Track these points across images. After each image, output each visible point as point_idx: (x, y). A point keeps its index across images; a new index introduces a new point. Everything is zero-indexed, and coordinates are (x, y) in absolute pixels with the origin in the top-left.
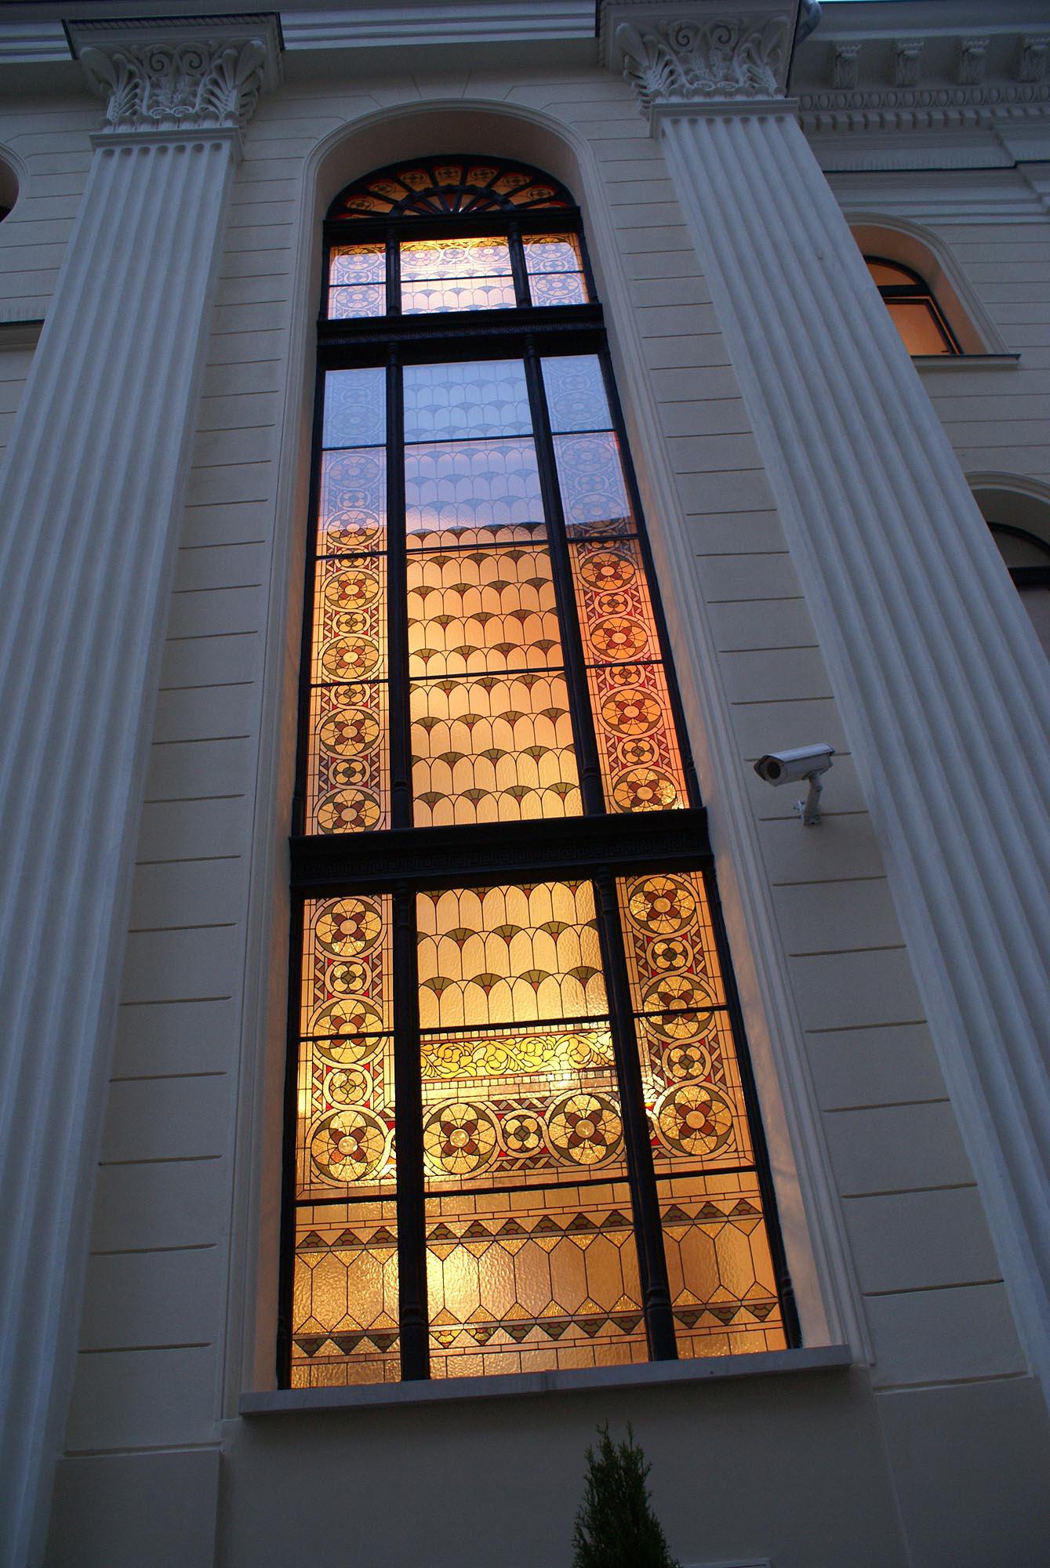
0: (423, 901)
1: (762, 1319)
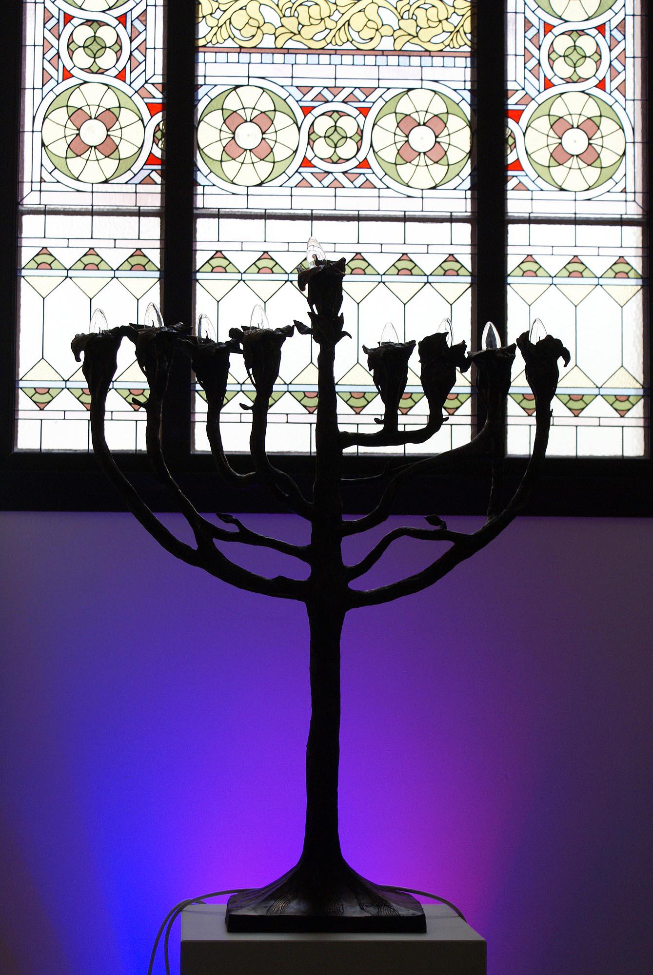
1: (622, 414)
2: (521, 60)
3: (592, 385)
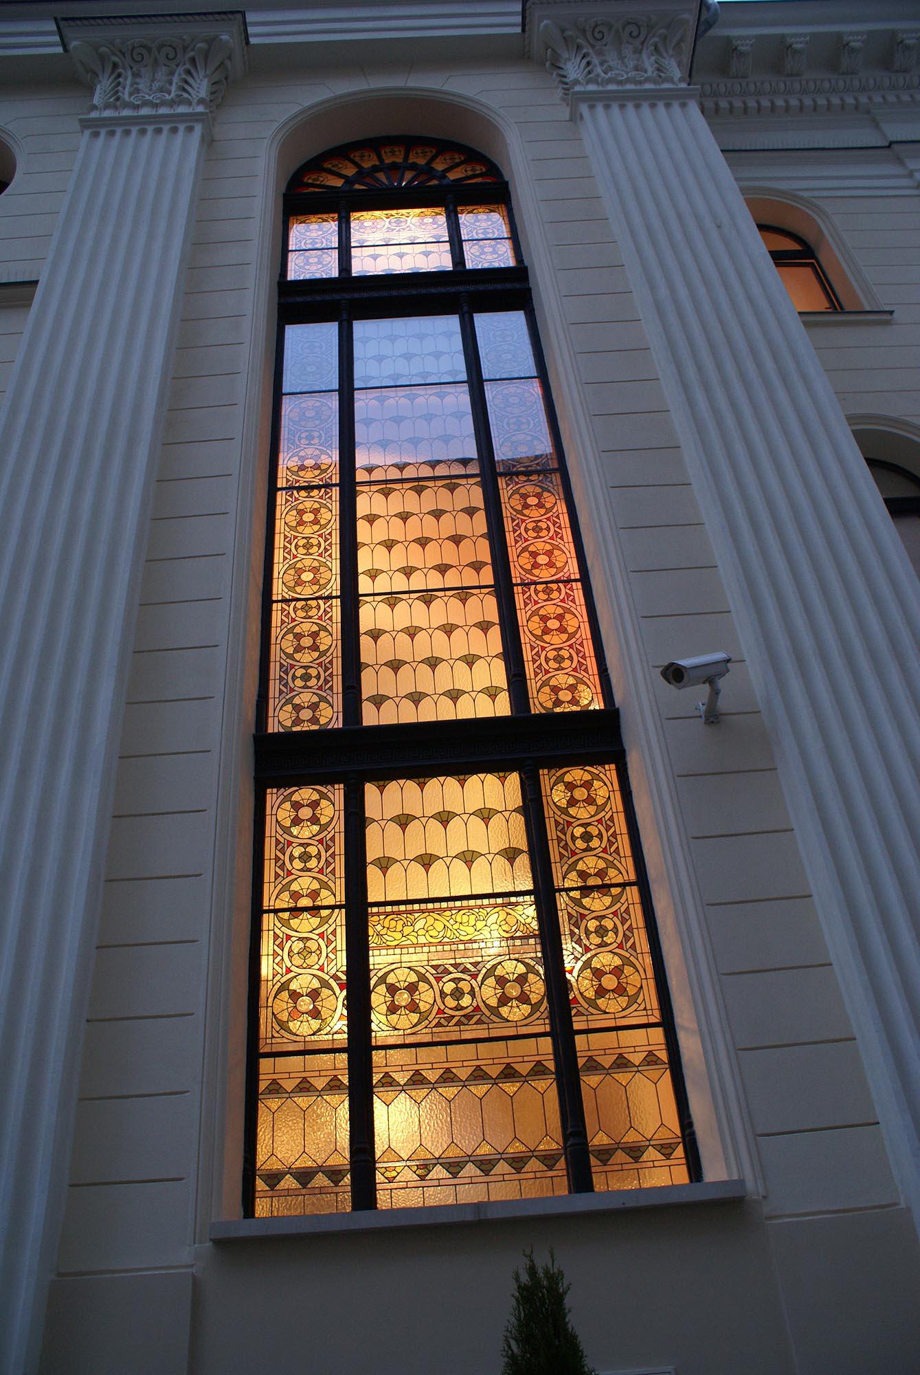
0: (370, 790)
1: (668, 1156)
2: (271, 958)
3: (493, 1151)
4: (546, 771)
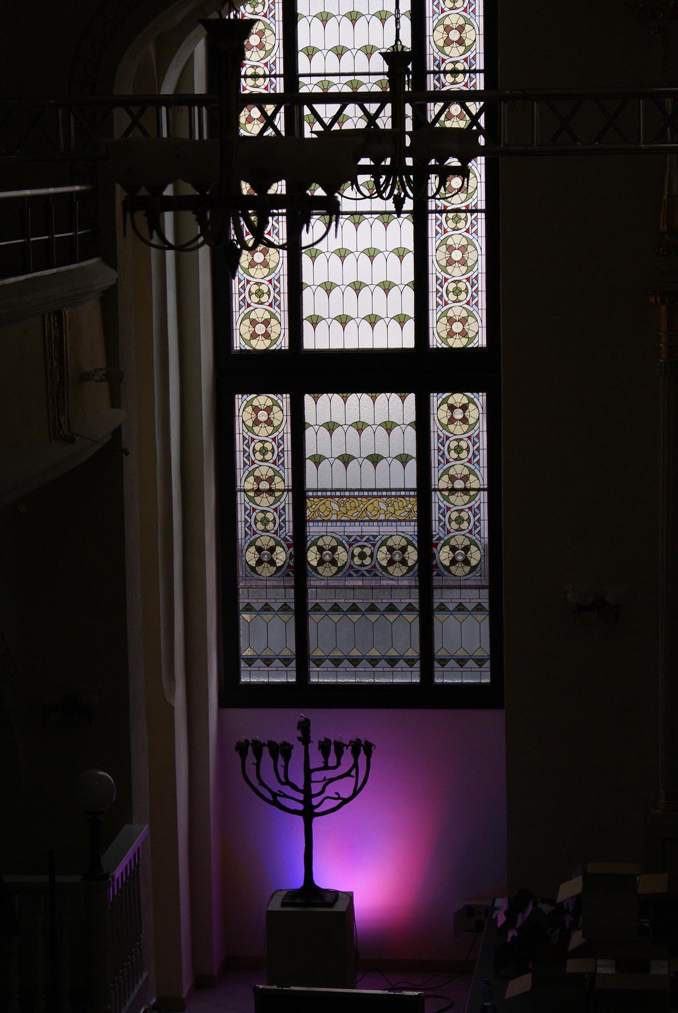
0: (308, 399)
1: (480, 666)
4: (240, 396)
